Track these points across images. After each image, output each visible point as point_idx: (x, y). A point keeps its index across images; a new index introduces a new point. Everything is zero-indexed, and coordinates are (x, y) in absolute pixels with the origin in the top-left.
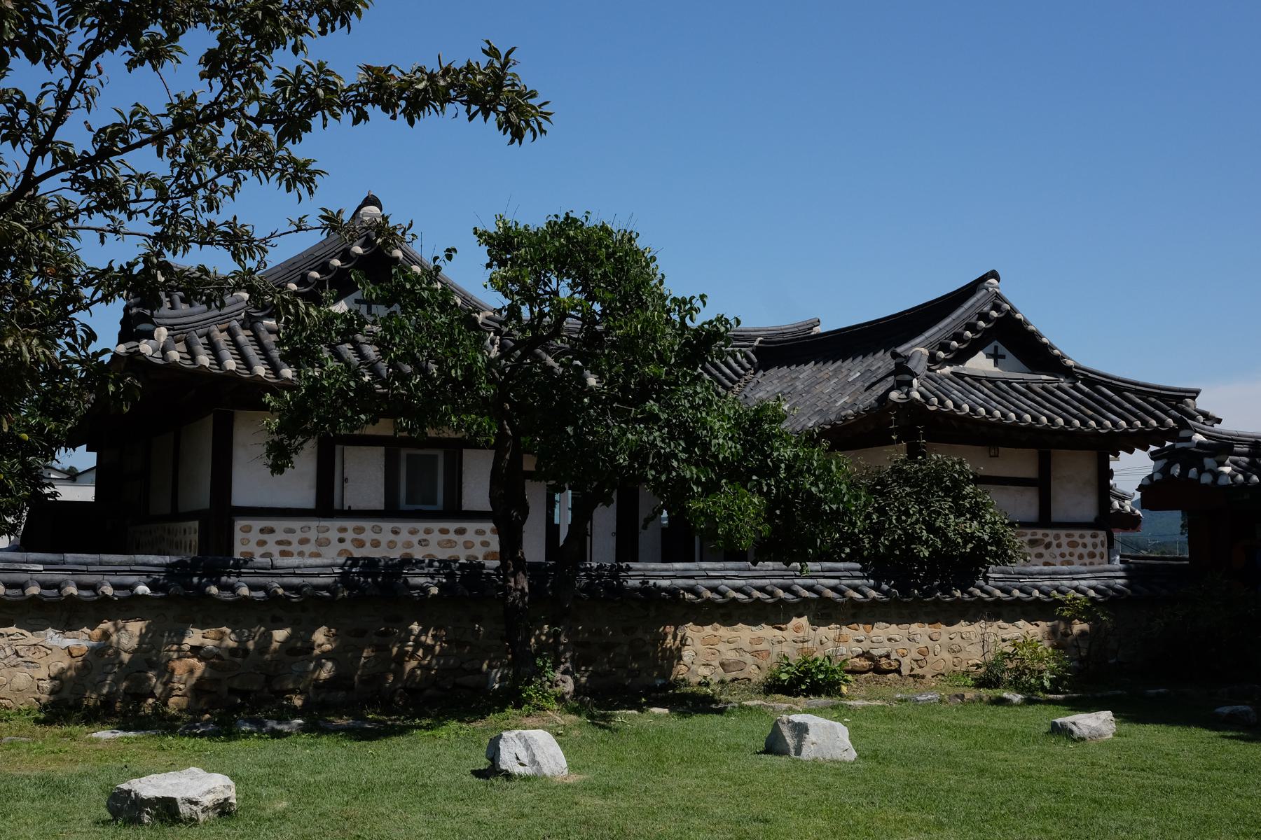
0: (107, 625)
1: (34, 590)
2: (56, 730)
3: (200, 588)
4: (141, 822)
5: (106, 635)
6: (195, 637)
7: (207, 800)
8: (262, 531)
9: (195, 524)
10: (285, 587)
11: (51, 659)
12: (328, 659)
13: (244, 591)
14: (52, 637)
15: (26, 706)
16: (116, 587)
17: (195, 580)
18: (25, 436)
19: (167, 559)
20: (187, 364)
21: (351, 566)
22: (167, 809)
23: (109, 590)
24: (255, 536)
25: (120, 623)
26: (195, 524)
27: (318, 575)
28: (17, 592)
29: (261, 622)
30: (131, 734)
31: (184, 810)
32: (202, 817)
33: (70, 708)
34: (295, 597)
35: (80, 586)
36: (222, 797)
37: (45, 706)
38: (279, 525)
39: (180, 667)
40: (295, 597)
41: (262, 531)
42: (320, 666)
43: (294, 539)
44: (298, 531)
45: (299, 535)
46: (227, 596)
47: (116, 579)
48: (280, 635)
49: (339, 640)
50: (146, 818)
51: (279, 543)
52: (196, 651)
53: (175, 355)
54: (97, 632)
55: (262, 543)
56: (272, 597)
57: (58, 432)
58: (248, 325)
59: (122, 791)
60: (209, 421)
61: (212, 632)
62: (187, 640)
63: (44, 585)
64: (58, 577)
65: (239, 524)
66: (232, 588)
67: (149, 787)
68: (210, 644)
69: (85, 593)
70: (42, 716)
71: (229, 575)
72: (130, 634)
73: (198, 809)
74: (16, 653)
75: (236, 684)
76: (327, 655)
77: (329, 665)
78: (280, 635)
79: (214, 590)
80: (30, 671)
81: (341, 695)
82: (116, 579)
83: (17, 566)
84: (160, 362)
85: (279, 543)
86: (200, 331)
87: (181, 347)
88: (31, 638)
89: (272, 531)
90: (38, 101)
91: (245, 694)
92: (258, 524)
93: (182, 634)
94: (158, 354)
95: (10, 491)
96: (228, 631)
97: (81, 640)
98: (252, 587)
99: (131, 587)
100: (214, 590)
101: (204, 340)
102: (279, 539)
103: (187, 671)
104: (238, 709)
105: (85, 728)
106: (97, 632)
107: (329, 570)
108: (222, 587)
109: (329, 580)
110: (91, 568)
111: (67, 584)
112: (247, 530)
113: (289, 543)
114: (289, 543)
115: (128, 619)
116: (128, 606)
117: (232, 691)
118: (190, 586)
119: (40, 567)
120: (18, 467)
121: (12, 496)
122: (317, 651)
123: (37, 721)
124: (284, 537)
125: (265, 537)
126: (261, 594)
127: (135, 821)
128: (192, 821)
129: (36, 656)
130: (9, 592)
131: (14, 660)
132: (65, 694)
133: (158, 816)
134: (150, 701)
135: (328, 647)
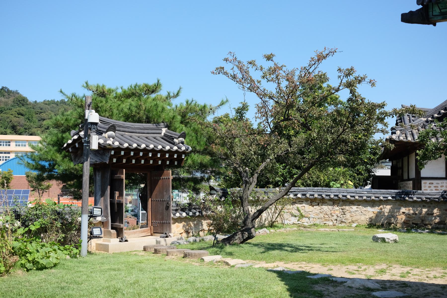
0: (381, 206)
1: (365, 198)
2: (370, 229)
3: (404, 198)
4: (378, 242)
5: (381, 209)
6: (403, 210)
7: (392, 239)
8: (430, 184)
9: (411, 182)
10: (426, 198)
11: (369, 214)
12: (438, 216)
13: (415, 199)
14: (369, 209)
15: (364, 224)
16: (384, 197)
17: (403, 196)
18: (366, 160)
19: (396, 191)
20: (405, 140)
21: (444, 193)
22: (383, 240)
23: (382, 198)
24: (428, 185)
25: (385, 206)
26: (411, 182)
27: (435, 195)
28: (361, 198)
29: (420, 206)
30: (387, 231)
31: (387, 240)
32: (390, 242)
33: (374, 225)
34: (428, 200)
35: (375, 197)
36: (395, 239)
37: (368, 225)
38: (435, 182)
39: (399, 217)
40: (428, 200)
41: (430, 184)
42: (435, 218)
43: (439, 186)
44: (440, 184)
45: (440, 185)
46: (411, 200)
47: (384, 196)
48: (425, 210)
49: (440, 213)
50: (379, 241)
51: (435, 187)
52: (403, 213)
53: (401, 138)
54: (380, 208)
55: (430, 187)
56: (423, 201)
57: (374, 159)
58: (423, 127)
59: (375, 236)
60: (407, 157)
61: (407, 209)
62: (401, 210)
63: (367, 197)
64: (370, 195)
65: (423, 182)
66: (412, 198)
67: (379, 236)
68: (407, 212)
69: (377, 199)
70: (367, 227)
71: (411, 195)
72: (387, 209)
73: (390, 240)
74: (361, 212)
75: (414, 222)
76: (438, 216)
77: (438, 218)
78: (425, 210)
79: (407, 198)
80: (365, 216)
81: (442, 226)
82: (384, 196)
83: (361, 192)
84: (398, 140)
85: (435, 187)
86: (409, 130)
87: (404, 135)
88: (365, 209)
89: (432, 184)
90: (296, 216)
91: (416, 224)
92: (428, 182)
93: (400, 209)
94: (397, 138)
95: (363, 174)
96: (412, 209)
97: (376, 209)
98: (418, 198)
99: (387, 197)
100: (407, 198)
101: (411, 133)
102: (435, 186)
103: (401, 218)
104: (413, 227)
105: (376, 229)
106: (380, 208)
107: (438, 194)
108: (409, 198)
109: (438, 196)
110: (378, 193)
111: (372, 196)
112: (425, 183)
113: (438, 187)
114: (438, 187)
115: (386, 205)
116: (387, 202)
117: (413, 223)
118: (401, 197)
119: (366, 193)
120: (364, 168)
121: (363, 175)
122: (435, 215)
123: (366, 228)
124: (436, 185)
125: (430, 185)
126: (420, 199)
127: (377, 241)
128: (389, 243)
129: (366, 213)
130: (359, 198)
131: (361, 214)
132: (373, 222)
133: (382, 241)
134: (393, 225)
135: (438, 214)
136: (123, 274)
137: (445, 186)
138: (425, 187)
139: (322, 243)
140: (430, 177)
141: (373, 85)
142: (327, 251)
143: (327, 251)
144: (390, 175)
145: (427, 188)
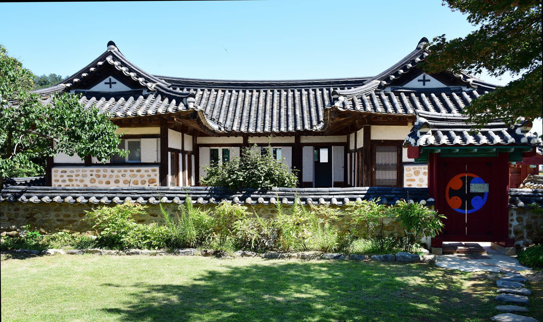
8: (62, 172)
24: (59, 174)
41: (62, 172)
44: (75, 172)
45: (75, 173)
51: (68, 176)
55: (62, 176)
65: (406, 167)
85: (68, 176)
89: (66, 172)
92: (60, 169)
102: (68, 175)
113: (72, 176)
114: (72, 176)
124: (70, 174)
125: (63, 174)
136: (381, 119)
137: (81, 175)
138: (55, 176)
139: (110, 282)
140: (65, 163)
141: (443, 5)
142: (109, 285)
143: (109, 285)
144: (327, 161)
145: (58, 178)
